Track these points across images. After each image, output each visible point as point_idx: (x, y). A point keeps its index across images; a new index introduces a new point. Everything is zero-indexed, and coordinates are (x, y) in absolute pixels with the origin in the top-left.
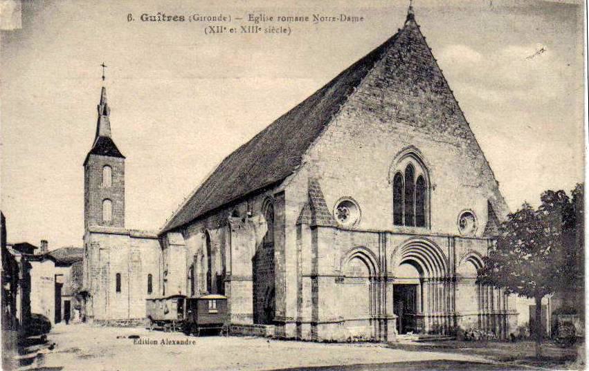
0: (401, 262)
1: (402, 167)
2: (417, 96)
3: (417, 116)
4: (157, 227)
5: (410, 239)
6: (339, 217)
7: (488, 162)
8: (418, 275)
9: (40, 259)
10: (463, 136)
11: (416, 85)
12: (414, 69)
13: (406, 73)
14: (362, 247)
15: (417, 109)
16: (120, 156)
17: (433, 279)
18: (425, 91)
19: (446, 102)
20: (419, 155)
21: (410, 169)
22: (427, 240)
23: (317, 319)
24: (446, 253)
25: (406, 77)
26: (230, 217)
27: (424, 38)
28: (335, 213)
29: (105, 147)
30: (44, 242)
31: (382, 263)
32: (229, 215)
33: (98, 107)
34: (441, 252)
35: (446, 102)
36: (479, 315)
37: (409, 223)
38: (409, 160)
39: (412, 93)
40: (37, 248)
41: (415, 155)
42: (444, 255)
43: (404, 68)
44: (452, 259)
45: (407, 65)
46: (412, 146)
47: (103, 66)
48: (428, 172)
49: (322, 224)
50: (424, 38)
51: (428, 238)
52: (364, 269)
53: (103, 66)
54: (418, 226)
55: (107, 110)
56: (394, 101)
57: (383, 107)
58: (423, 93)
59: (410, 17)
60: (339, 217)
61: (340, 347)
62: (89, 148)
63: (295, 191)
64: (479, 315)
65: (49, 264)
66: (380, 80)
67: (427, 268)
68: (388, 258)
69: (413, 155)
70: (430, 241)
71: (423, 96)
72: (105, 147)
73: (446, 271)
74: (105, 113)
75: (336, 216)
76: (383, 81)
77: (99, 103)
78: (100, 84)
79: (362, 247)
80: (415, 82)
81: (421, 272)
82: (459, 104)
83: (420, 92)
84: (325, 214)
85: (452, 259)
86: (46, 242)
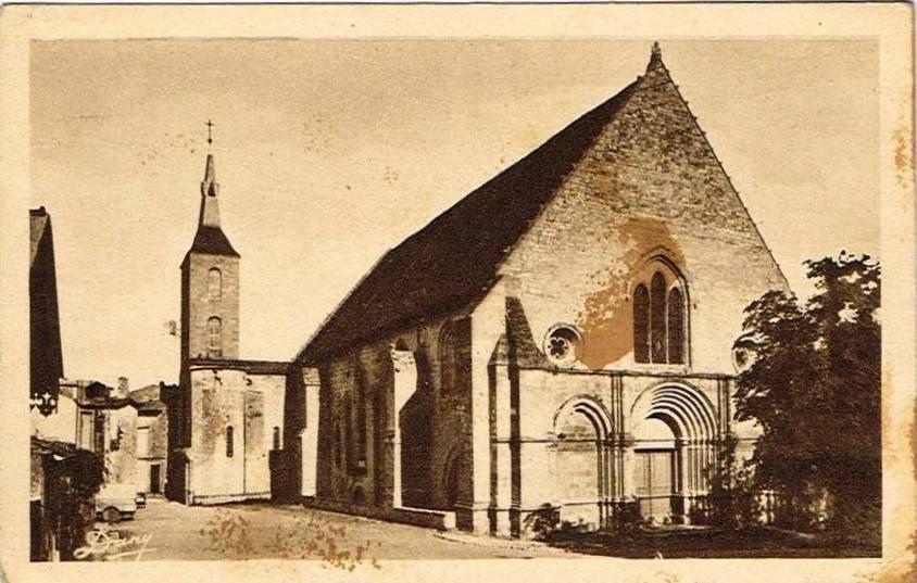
0: (649, 414)
1: (647, 277)
2: (668, 172)
3: (668, 201)
4: (288, 352)
5: (660, 383)
6: (553, 353)
7: (778, 265)
8: (671, 435)
9: (117, 404)
10: (739, 228)
11: (666, 155)
12: (663, 133)
13: (651, 138)
14: (587, 396)
15: (668, 191)
16: (234, 254)
17: (696, 442)
18: (679, 164)
19: (711, 179)
20: (672, 258)
21: (659, 276)
22: (684, 383)
23: (496, 506)
24: (715, 403)
25: (650, 145)
26: (393, 351)
27: (676, 87)
28: (546, 347)
29: (211, 241)
30: (123, 379)
31: (618, 417)
32: (391, 347)
33: (203, 184)
34: (708, 401)
35: (711, 179)
36: (600, 504)
37: (659, 360)
38: (658, 266)
39: (660, 168)
40: (112, 389)
41: (666, 258)
42: (711, 406)
43: (647, 132)
44: (723, 411)
45: (652, 127)
46: (663, 247)
47: (210, 124)
48: (686, 282)
49: (522, 366)
50: (676, 87)
51: (688, 380)
52: (591, 429)
53: (210, 124)
54: (671, 363)
55: (215, 188)
56: (634, 181)
57: (616, 191)
58: (677, 167)
59: (656, 58)
60: (553, 353)
61: (254, 513)
62: (189, 247)
63: (488, 323)
64: (600, 504)
65: (130, 411)
66: (612, 150)
67: (685, 423)
68: (626, 413)
69: (664, 259)
70: (694, 388)
71: (677, 170)
72: (211, 241)
73: (716, 431)
74: (212, 193)
75: (548, 351)
76: (615, 152)
77: (203, 179)
78: (204, 149)
79: (587, 396)
80: (665, 151)
81: (676, 431)
82: (732, 180)
83: (673, 166)
84: (714, 166)
85: (723, 411)
86: (125, 379)
